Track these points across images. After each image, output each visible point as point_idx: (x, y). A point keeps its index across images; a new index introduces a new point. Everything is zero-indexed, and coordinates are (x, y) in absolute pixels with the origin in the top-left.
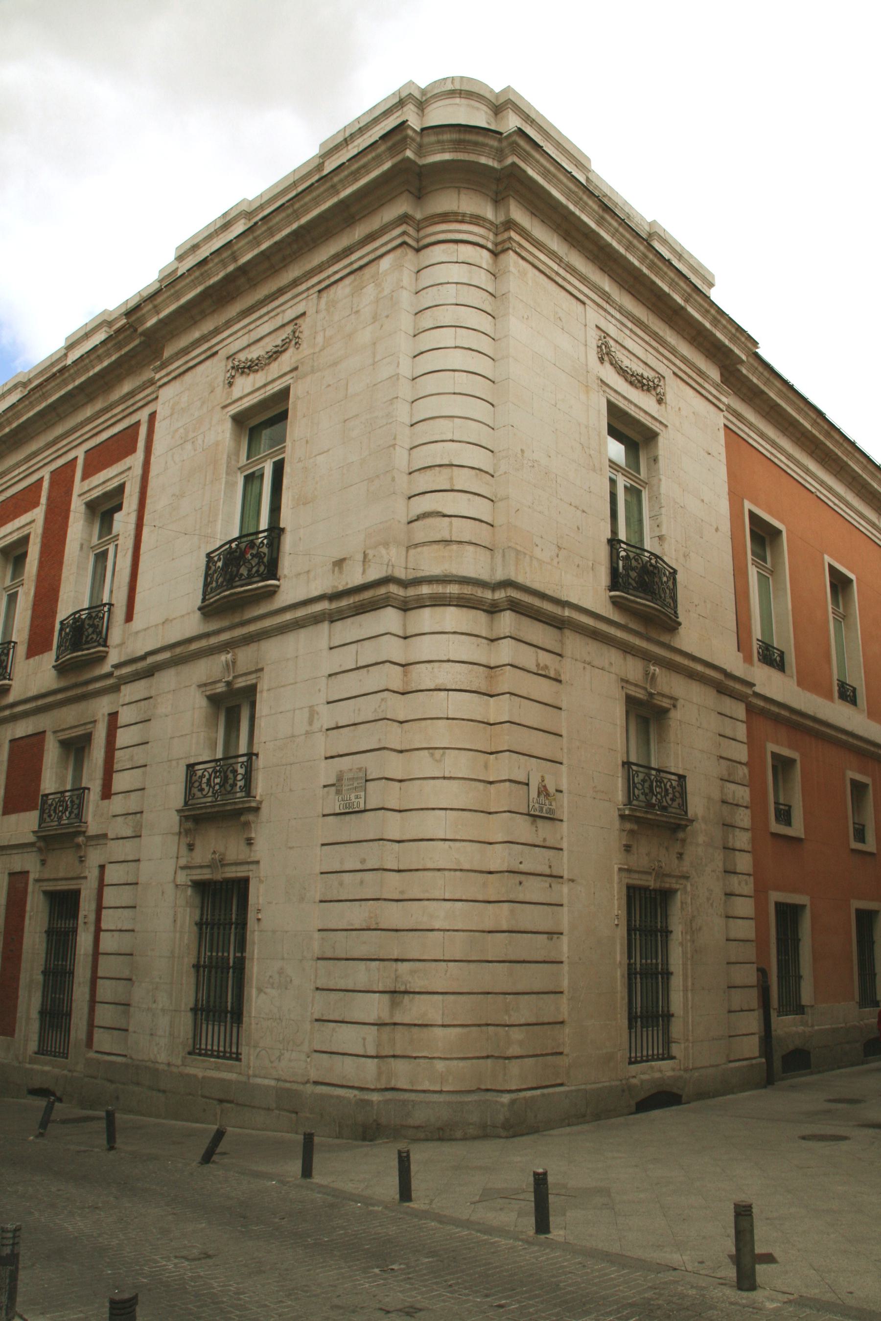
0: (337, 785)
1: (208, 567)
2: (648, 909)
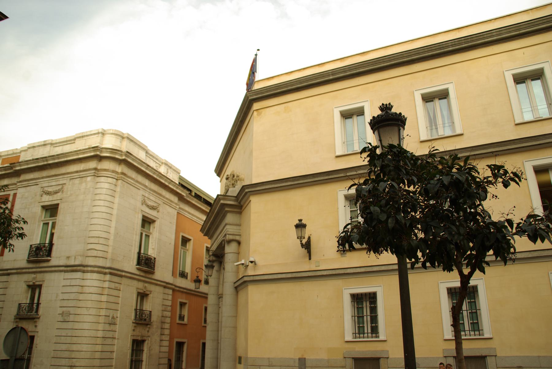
0: (62, 314)
1: (30, 249)
2: (137, 345)
